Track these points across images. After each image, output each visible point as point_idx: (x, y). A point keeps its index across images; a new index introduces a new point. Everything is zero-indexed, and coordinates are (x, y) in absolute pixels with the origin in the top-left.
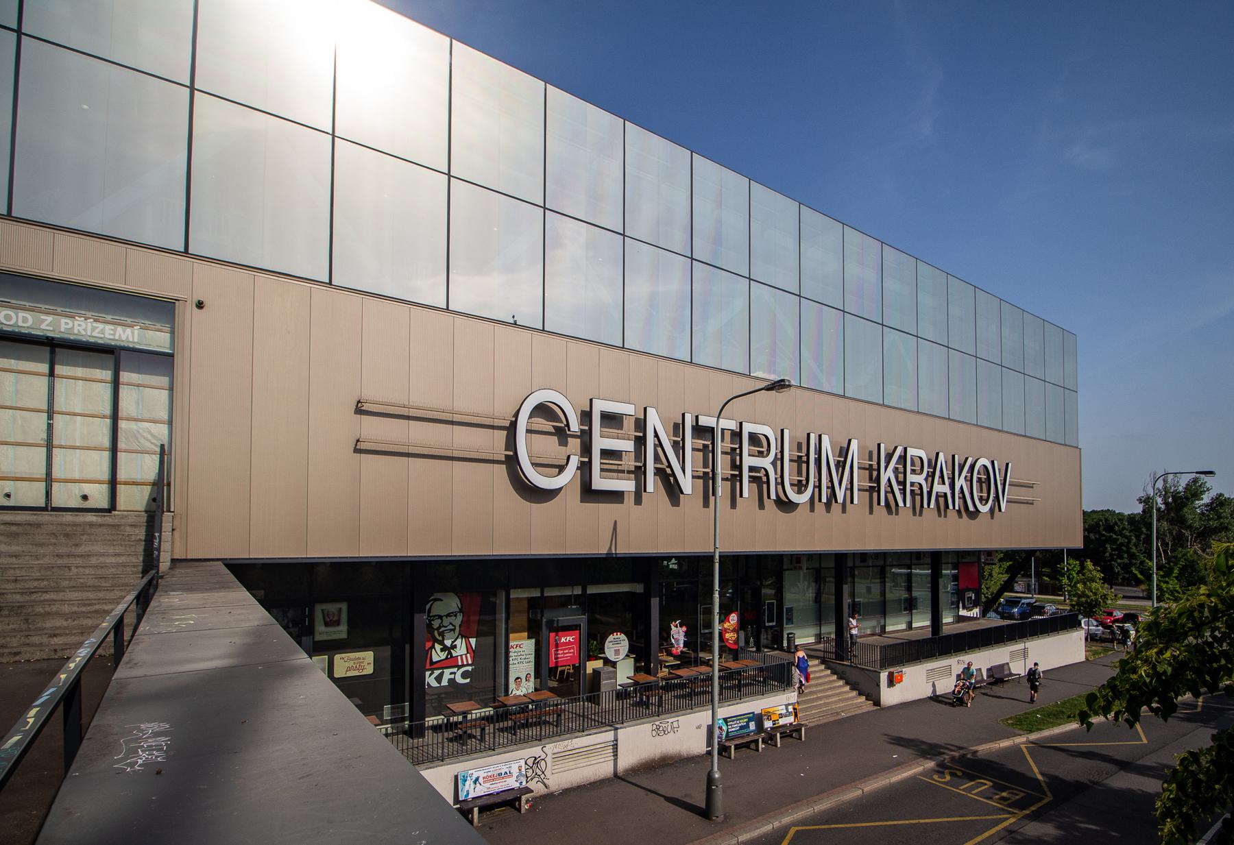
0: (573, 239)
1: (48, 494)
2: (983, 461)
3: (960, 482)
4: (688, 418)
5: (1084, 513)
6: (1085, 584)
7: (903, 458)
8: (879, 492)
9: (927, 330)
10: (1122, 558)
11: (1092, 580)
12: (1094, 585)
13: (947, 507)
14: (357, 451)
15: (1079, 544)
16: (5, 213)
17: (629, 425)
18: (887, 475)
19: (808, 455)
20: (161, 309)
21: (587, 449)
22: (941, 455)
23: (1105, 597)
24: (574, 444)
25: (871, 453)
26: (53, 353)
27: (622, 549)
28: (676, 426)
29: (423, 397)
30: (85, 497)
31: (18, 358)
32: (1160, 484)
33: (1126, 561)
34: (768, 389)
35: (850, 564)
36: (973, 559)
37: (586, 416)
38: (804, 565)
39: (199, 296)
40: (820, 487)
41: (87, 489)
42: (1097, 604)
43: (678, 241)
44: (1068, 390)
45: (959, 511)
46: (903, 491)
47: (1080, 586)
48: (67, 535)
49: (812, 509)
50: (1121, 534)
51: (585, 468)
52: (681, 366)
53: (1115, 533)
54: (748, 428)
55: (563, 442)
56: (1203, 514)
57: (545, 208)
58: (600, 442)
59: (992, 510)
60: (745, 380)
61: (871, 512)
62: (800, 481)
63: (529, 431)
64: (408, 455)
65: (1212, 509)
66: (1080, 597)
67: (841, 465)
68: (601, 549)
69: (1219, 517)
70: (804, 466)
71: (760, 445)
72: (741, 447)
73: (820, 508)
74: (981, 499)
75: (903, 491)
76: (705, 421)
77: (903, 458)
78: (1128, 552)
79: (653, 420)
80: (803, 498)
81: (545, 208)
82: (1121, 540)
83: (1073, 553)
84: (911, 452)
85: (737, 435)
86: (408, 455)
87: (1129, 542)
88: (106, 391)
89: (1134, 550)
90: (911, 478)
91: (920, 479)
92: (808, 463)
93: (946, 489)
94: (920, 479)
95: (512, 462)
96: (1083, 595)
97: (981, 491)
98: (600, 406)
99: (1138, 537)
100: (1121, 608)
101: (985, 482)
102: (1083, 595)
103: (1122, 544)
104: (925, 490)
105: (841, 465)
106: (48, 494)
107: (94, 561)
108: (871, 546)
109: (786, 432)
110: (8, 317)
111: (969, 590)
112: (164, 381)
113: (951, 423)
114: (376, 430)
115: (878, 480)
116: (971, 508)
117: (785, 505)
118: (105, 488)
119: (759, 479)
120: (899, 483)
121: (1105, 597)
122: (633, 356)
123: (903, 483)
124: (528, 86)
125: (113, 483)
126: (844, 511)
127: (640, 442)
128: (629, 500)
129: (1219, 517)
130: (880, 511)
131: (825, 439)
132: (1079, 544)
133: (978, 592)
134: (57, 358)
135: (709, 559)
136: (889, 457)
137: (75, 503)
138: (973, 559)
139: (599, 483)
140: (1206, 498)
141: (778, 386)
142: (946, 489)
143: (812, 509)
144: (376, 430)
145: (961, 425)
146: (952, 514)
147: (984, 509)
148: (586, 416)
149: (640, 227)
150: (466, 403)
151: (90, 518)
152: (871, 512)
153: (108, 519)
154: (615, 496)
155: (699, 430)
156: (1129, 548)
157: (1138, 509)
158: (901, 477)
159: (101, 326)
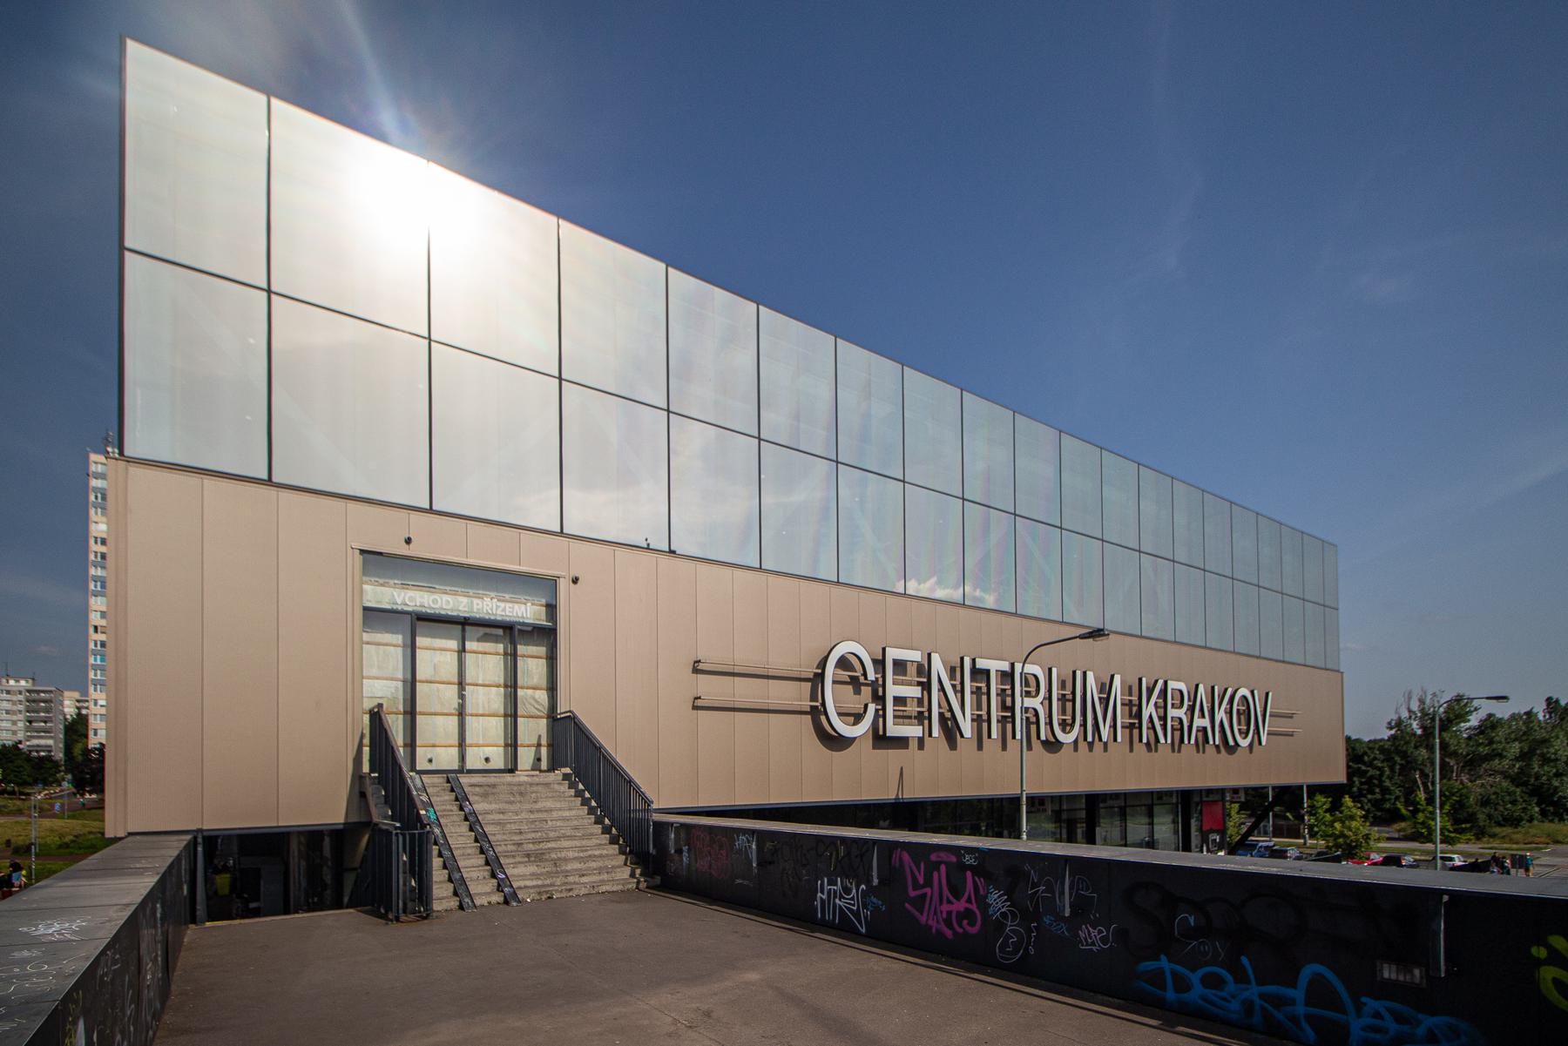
0: (693, 440)
1: (462, 758)
2: (1244, 691)
3: (1220, 715)
4: (967, 661)
5: (1348, 739)
6: (1343, 822)
7: (1164, 691)
8: (1140, 728)
9: (1181, 556)
10: (1373, 793)
11: (1352, 818)
12: (1354, 824)
13: (1182, 741)
14: (695, 708)
15: (1340, 777)
16: (265, 477)
17: (912, 670)
18: (1149, 710)
19: (1074, 693)
20: (545, 586)
21: (879, 699)
22: (1117, 679)
23: (1367, 837)
24: (866, 692)
25: (1130, 688)
26: (463, 630)
27: (909, 794)
28: (1103, 685)
29: (743, 657)
30: (487, 760)
31: (433, 636)
32: (1415, 706)
33: (1378, 796)
34: (1082, 637)
35: (1197, 799)
36: (1217, 797)
37: (880, 664)
38: (1049, 807)
39: (573, 574)
40: (1154, 728)
41: (489, 751)
42: (1358, 846)
43: (818, 439)
44: (1329, 608)
45: (1217, 747)
46: (1164, 727)
47: (1338, 825)
48: (521, 794)
49: (1076, 749)
50: (1370, 764)
51: (881, 714)
52: (826, 587)
53: (1364, 763)
54: (893, 654)
55: (857, 692)
56: (1469, 738)
57: (759, 439)
58: (893, 690)
59: (1251, 745)
60: (1056, 627)
61: (1131, 750)
62: (921, 713)
63: (834, 682)
64: (768, 711)
65: (1482, 732)
66: (1336, 837)
67: (1105, 702)
68: (890, 795)
69: (1491, 742)
70: (984, 698)
71: (852, 669)
72: (1013, 688)
73: (1082, 745)
74: (1063, 724)
75: (1164, 727)
76: (982, 664)
77: (1164, 691)
78: (1380, 785)
79: (938, 666)
80: (1244, 743)
81: (759, 439)
82: (1372, 772)
83: (1334, 792)
84: (1172, 685)
85: (1008, 676)
86: (768, 711)
87: (1381, 775)
88: (451, 659)
89: (1387, 783)
90: (1172, 712)
91: (1035, 703)
92: (1074, 701)
93: (1206, 722)
94: (1181, 713)
95: (817, 712)
96: (1342, 835)
97: (1064, 712)
98: (893, 654)
99: (1392, 769)
100: (1379, 851)
101: (1246, 714)
102: (1342, 835)
103: (1372, 777)
104: (1186, 724)
105: (1105, 702)
106: (462, 758)
107: (555, 814)
108: (1131, 786)
109: (1054, 670)
110: (435, 601)
111: (1213, 831)
112: (542, 650)
113: (1018, 620)
114: (711, 689)
115: (1139, 715)
116: (1231, 743)
117: (1053, 745)
118: (455, 751)
119: (1032, 720)
120: (1160, 718)
121: (1367, 837)
122: (771, 578)
123: (1163, 719)
124: (650, 268)
125: (462, 744)
126: (1106, 749)
127: (926, 687)
128: (913, 744)
129: (1491, 742)
130: (1140, 748)
131: (1090, 675)
132: (1340, 777)
133: (1222, 831)
134: (467, 635)
135: (1015, 801)
136: (1150, 691)
137: (480, 765)
138: (1217, 797)
139: (893, 730)
140: (1474, 721)
141: (1096, 634)
142: (1206, 722)
143: (1076, 749)
144: (711, 689)
145: (924, 603)
146: (1210, 749)
147: (1244, 743)
148: (880, 664)
149: (776, 422)
150: (780, 661)
151: (492, 779)
152: (1131, 750)
153: (508, 778)
154: (902, 742)
155: (977, 673)
156: (1381, 782)
157: (1386, 734)
158: (1161, 711)
159: (502, 605)
